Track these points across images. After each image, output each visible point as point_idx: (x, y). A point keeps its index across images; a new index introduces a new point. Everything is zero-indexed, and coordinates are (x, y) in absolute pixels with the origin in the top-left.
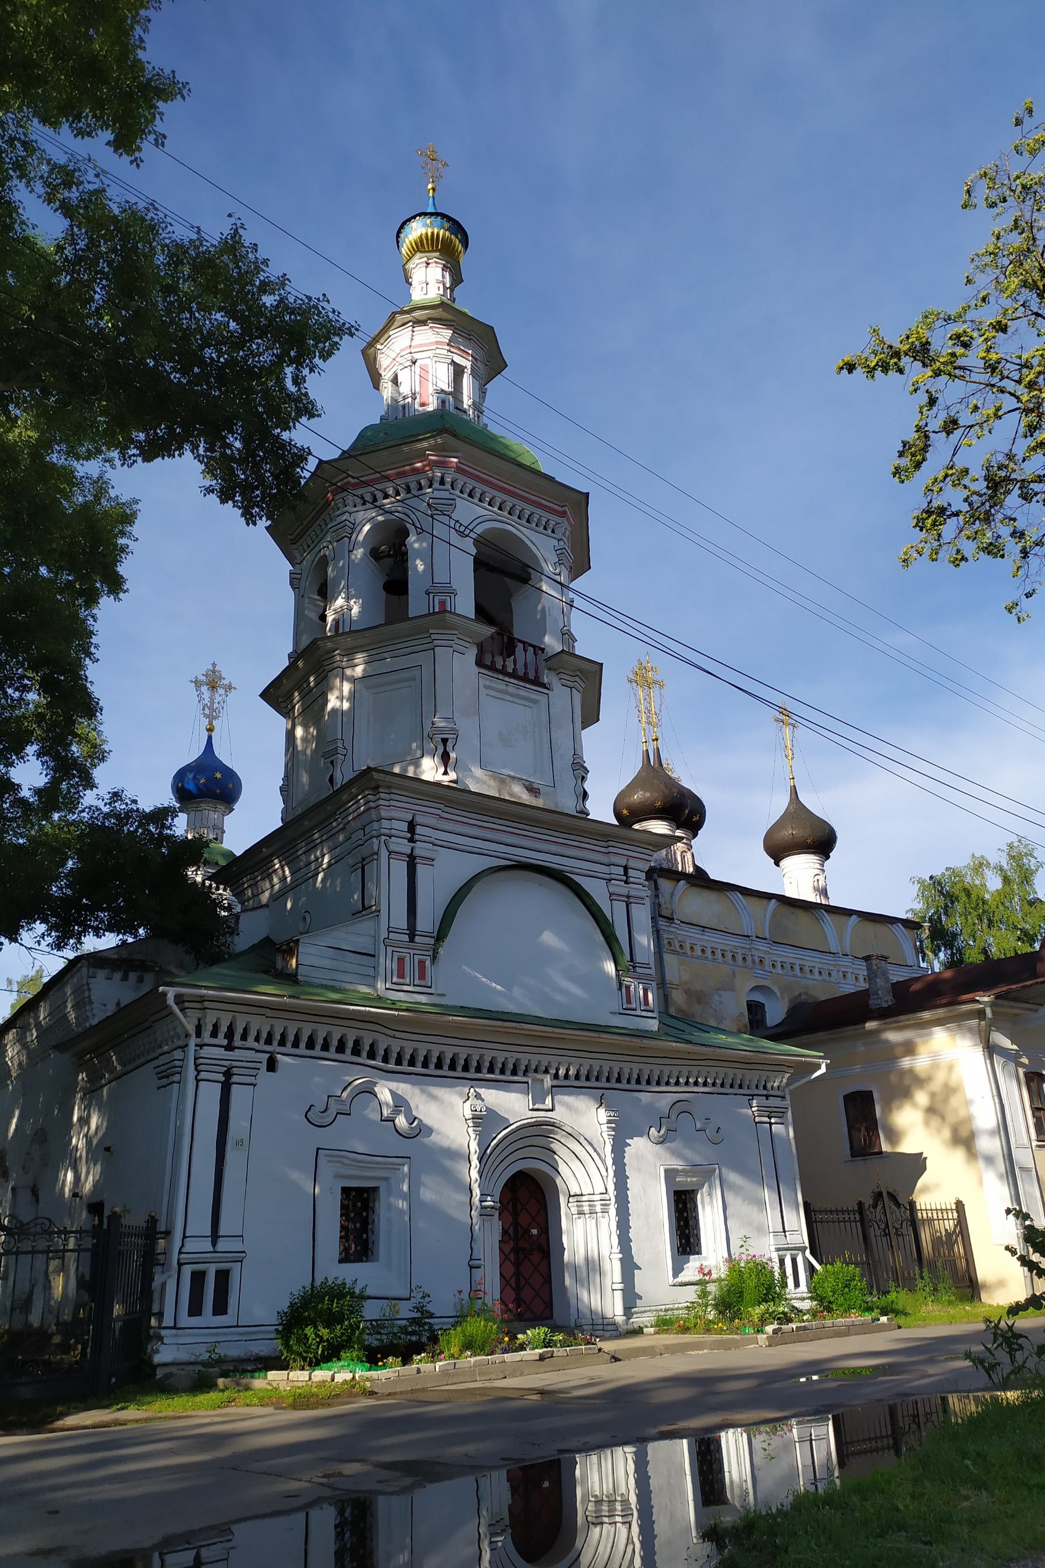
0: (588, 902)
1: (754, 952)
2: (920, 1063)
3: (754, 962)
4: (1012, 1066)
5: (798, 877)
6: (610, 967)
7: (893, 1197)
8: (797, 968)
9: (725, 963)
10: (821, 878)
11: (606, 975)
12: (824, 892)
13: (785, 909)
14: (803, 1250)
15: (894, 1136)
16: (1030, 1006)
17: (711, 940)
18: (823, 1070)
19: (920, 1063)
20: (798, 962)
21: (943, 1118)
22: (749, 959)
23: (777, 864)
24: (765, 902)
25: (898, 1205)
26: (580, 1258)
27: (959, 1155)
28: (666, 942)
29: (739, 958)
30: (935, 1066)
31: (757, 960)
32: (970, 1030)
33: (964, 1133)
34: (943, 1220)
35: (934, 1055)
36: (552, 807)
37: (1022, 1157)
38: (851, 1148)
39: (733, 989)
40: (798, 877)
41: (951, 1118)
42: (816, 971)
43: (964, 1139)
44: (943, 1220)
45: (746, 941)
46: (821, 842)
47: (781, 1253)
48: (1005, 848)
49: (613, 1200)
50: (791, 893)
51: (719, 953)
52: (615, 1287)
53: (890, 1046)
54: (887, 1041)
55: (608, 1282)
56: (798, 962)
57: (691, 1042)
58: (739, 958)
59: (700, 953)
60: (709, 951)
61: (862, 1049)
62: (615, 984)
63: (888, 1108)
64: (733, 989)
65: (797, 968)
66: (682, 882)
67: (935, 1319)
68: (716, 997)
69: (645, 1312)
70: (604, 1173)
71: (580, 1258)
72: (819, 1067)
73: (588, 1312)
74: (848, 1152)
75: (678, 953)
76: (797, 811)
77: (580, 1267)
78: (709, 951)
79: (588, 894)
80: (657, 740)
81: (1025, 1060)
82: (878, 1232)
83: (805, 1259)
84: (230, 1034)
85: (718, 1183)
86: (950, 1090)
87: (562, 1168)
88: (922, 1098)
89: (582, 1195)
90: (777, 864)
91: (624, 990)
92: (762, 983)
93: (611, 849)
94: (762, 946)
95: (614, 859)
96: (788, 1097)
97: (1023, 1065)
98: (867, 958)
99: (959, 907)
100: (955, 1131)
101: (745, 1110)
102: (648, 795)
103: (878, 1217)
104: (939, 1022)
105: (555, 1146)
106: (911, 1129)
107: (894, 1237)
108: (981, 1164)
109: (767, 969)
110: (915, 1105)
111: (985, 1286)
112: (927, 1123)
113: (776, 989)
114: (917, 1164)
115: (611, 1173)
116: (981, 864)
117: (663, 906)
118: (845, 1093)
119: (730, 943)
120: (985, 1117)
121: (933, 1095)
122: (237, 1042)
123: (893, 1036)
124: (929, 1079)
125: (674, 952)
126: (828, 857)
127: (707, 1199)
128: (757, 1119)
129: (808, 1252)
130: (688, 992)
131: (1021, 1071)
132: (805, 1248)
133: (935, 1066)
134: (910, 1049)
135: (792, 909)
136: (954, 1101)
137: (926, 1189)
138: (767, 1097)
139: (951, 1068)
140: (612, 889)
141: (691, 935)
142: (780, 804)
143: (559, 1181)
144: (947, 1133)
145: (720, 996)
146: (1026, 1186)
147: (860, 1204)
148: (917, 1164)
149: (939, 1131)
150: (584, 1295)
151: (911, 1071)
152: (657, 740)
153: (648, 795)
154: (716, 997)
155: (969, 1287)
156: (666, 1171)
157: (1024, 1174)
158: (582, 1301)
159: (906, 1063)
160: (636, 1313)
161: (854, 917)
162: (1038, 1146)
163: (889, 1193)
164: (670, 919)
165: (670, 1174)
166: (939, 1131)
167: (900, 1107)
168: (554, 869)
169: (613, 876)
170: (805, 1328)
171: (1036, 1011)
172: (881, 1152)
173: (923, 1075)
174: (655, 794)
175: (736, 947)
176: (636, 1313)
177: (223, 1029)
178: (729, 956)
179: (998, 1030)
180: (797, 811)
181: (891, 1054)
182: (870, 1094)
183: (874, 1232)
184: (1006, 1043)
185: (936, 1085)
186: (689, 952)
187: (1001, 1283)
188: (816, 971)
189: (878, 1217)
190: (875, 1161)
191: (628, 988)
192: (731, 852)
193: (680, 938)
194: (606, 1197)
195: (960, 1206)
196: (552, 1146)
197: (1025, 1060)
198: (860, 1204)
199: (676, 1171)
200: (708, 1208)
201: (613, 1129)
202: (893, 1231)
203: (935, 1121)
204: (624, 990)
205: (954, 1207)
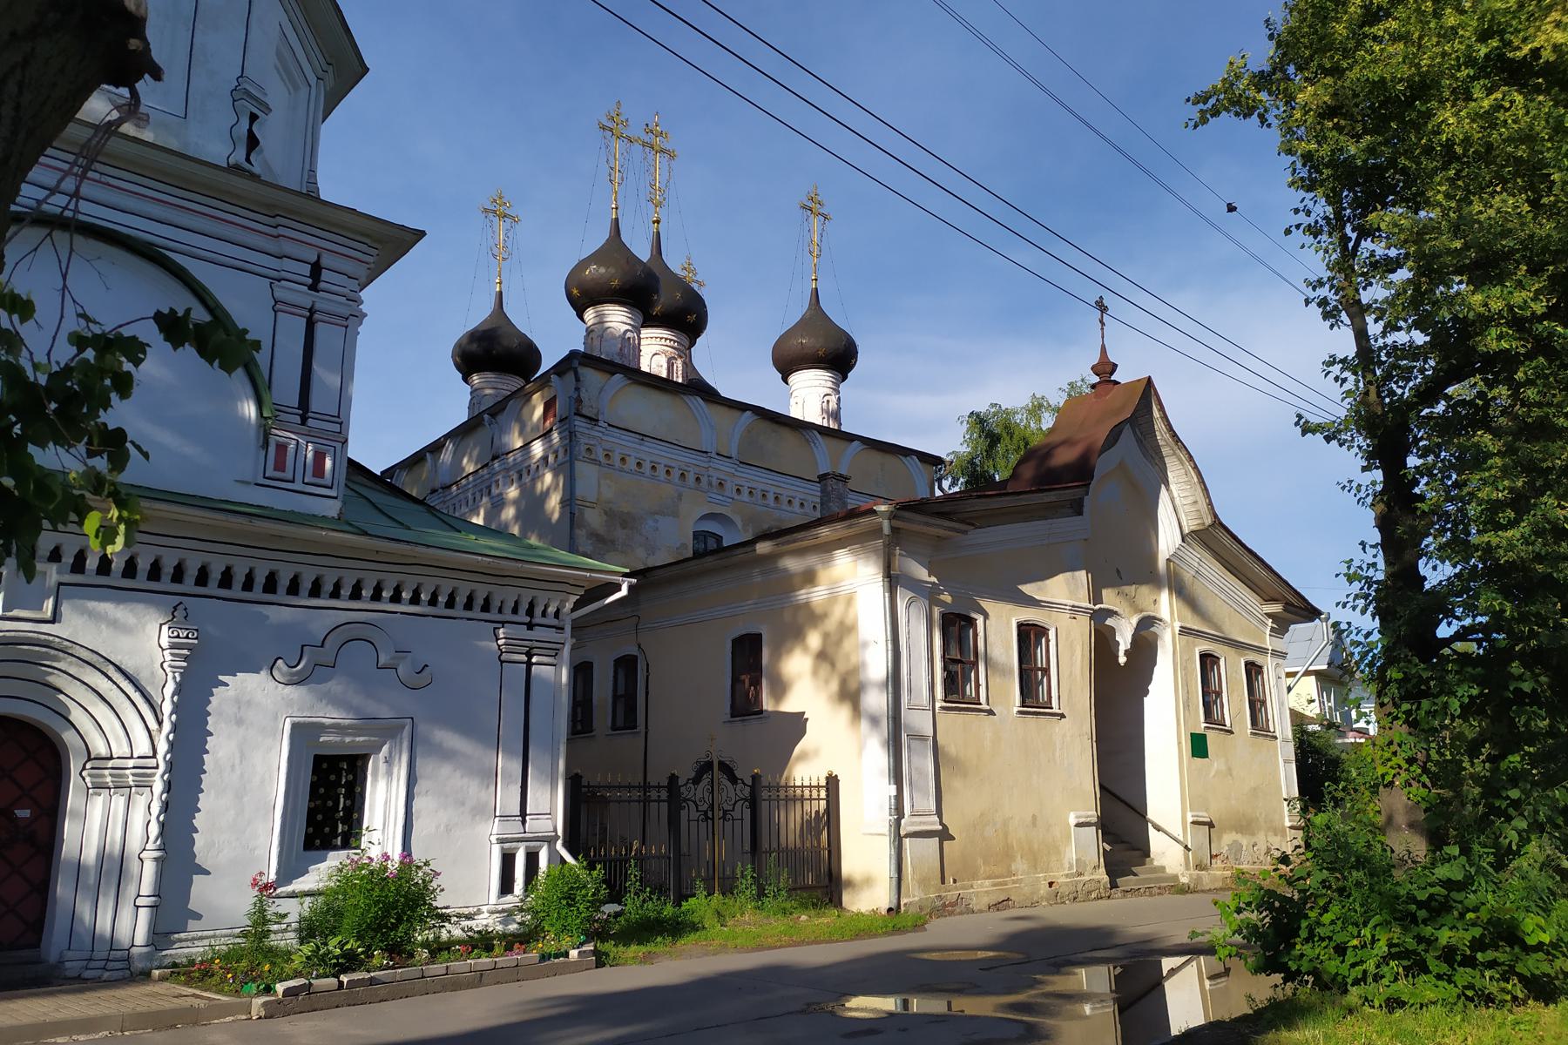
0: (210, 303)
1: (711, 472)
2: (816, 595)
3: (710, 484)
4: (922, 604)
5: (808, 395)
6: (250, 410)
7: (727, 769)
8: (771, 497)
9: (669, 482)
10: (833, 399)
11: (244, 421)
12: (836, 415)
13: (765, 426)
14: (551, 841)
15: (781, 688)
16: (957, 525)
17: (650, 452)
18: (624, 592)
19: (816, 595)
20: (773, 489)
21: (833, 665)
22: (704, 480)
23: (785, 380)
24: (736, 413)
25: (734, 779)
26: (90, 855)
27: (845, 712)
28: (583, 448)
29: (691, 478)
30: (833, 599)
31: (715, 482)
32: (875, 551)
33: (853, 685)
34: (811, 799)
35: (834, 585)
36: (174, 144)
37: (917, 720)
38: (732, 706)
39: (675, 514)
40: (808, 395)
41: (842, 666)
42: (796, 503)
43: (850, 694)
44: (811, 799)
45: (703, 458)
46: (839, 359)
47: (507, 845)
48: (1066, 387)
49: (162, 767)
50: (795, 413)
51: (661, 471)
52: (140, 902)
53: (787, 576)
54: (786, 570)
55: (131, 891)
56: (773, 489)
57: (365, 534)
58: (691, 478)
59: (634, 467)
60: (647, 467)
61: (759, 579)
62: (252, 437)
63: (778, 654)
64: (675, 514)
65: (771, 497)
66: (618, 376)
67: (735, 938)
68: (650, 522)
69: (201, 938)
70: (153, 725)
71: (90, 855)
72: (618, 588)
73: (88, 940)
74: (728, 710)
75: (600, 464)
76: (816, 316)
77: (87, 868)
78: (647, 467)
79: (205, 289)
80: (658, 222)
81: (947, 598)
82: (694, 815)
83: (553, 853)
84: (530, 612)
85: (406, 745)
86: (846, 629)
87: (77, 715)
88: (814, 640)
89: (111, 758)
90: (785, 380)
91: (272, 449)
92: (718, 510)
93: (281, 231)
94: (725, 467)
95: (288, 247)
96: (568, 628)
97: (942, 603)
98: (823, 478)
99: (1000, 448)
100: (844, 683)
101: (484, 643)
102: (602, 270)
103: (699, 795)
104: (840, 544)
105: (58, 680)
106: (801, 686)
107: (718, 823)
108: (864, 725)
109: (727, 493)
110: (806, 649)
111: (850, 884)
112: (815, 672)
113: (738, 520)
114: (796, 725)
115: (167, 726)
116: (1040, 406)
117: (586, 402)
118: (737, 634)
119: (680, 459)
120: (876, 666)
121: (826, 636)
122: (538, 619)
123: (792, 564)
124: (825, 616)
125: (595, 462)
126: (845, 378)
127: (382, 767)
128: (504, 656)
129: (559, 845)
130: (610, 514)
131: (937, 611)
132: (557, 837)
133: (833, 599)
134: (810, 578)
135: (775, 427)
136: (848, 645)
137: (804, 756)
138: (530, 626)
139: (850, 600)
140: (279, 294)
141: (622, 444)
142: (796, 312)
143: (69, 737)
144: (834, 686)
145: (656, 521)
146: (915, 759)
147: (673, 779)
148: (796, 725)
149: (827, 682)
150: (84, 910)
151: (807, 605)
152: (658, 222)
153: (602, 270)
154: (650, 522)
155: (827, 885)
156: (294, 726)
157: (915, 744)
158: (82, 921)
159: (802, 595)
160: (181, 941)
161: (856, 443)
162: (943, 708)
163: (721, 764)
164: (593, 420)
165: (302, 733)
166: (827, 682)
167: (790, 651)
168: (129, 237)
169: (284, 274)
170: (372, 981)
171: (965, 532)
172: (761, 712)
173: (819, 610)
174: (612, 270)
175: (688, 464)
176: (181, 941)
177: (524, 606)
178: (676, 474)
179: (912, 554)
180: (816, 316)
181: (789, 584)
182: (760, 635)
183: (688, 814)
184: (922, 573)
185: (831, 624)
186: (618, 463)
187: (868, 881)
188: (796, 503)
189: (699, 795)
190: (753, 724)
191: (281, 448)
192: (735, 362)
193: (607, 446)
194: (152, 762)
195: (832, 783)
196: (51, 679)
197: (947, 598)
198: (673, 779)
199: (321, 728)
200: (382, 784)
201: (186, 658)
202: (718, 814)
203: (825, 669)
204: (272, 449)
205: (823, 783)
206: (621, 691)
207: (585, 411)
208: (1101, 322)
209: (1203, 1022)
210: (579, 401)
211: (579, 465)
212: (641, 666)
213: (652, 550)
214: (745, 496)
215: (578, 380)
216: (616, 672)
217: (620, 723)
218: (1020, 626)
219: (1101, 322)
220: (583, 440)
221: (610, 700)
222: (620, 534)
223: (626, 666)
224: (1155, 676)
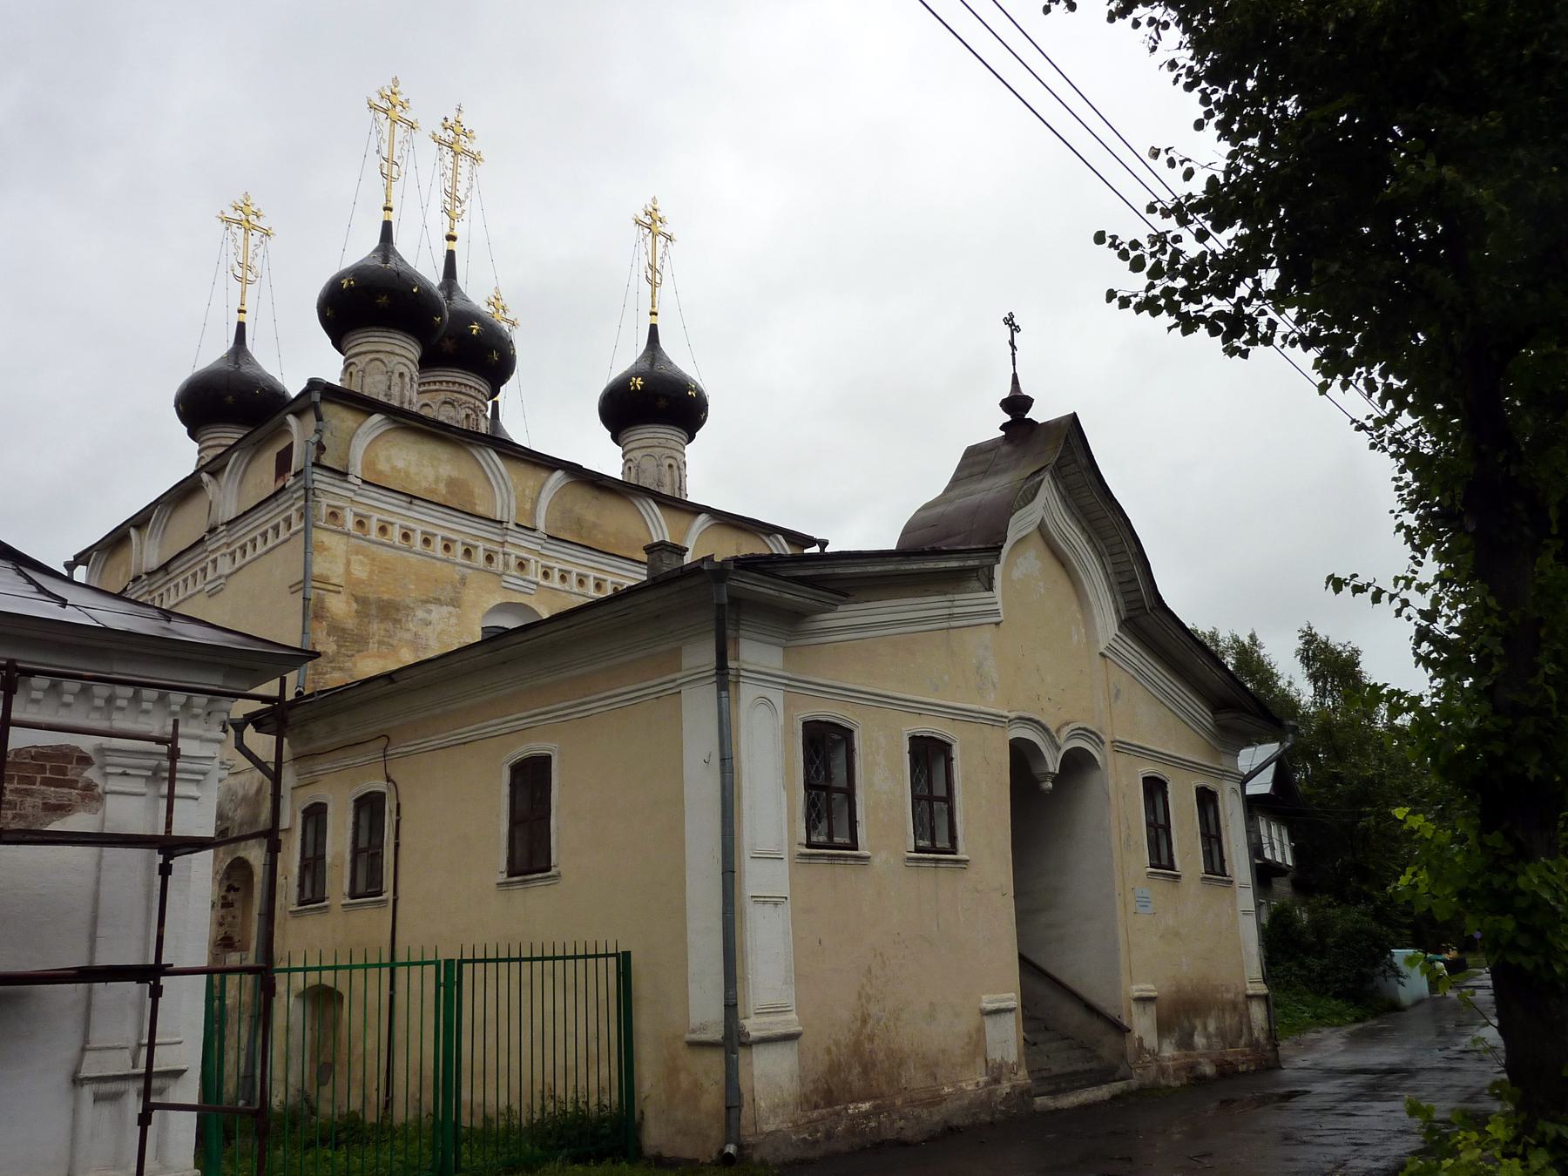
28: (324, 511)
39: (455, 602)
66: (377, 418)
75: (348, 534)
154: (420, 614)
186: (374, 535)
206: (363, 843)
207: (327, 460)
208: (1012, 344)
209: (96, 985)
210: (321, 448)
211: (318, 536)
212: (390, 805)
213: (415, 644)
214: (555, 582)
215: (319, 418)
216: (356, 824)
217: (361, 888)
218: (914, 740)
219: (1012, 344)
220: (325, 501)
221: (348, 857)
222: (376, 628)
223: (370, 807)
224: (518, 354)
